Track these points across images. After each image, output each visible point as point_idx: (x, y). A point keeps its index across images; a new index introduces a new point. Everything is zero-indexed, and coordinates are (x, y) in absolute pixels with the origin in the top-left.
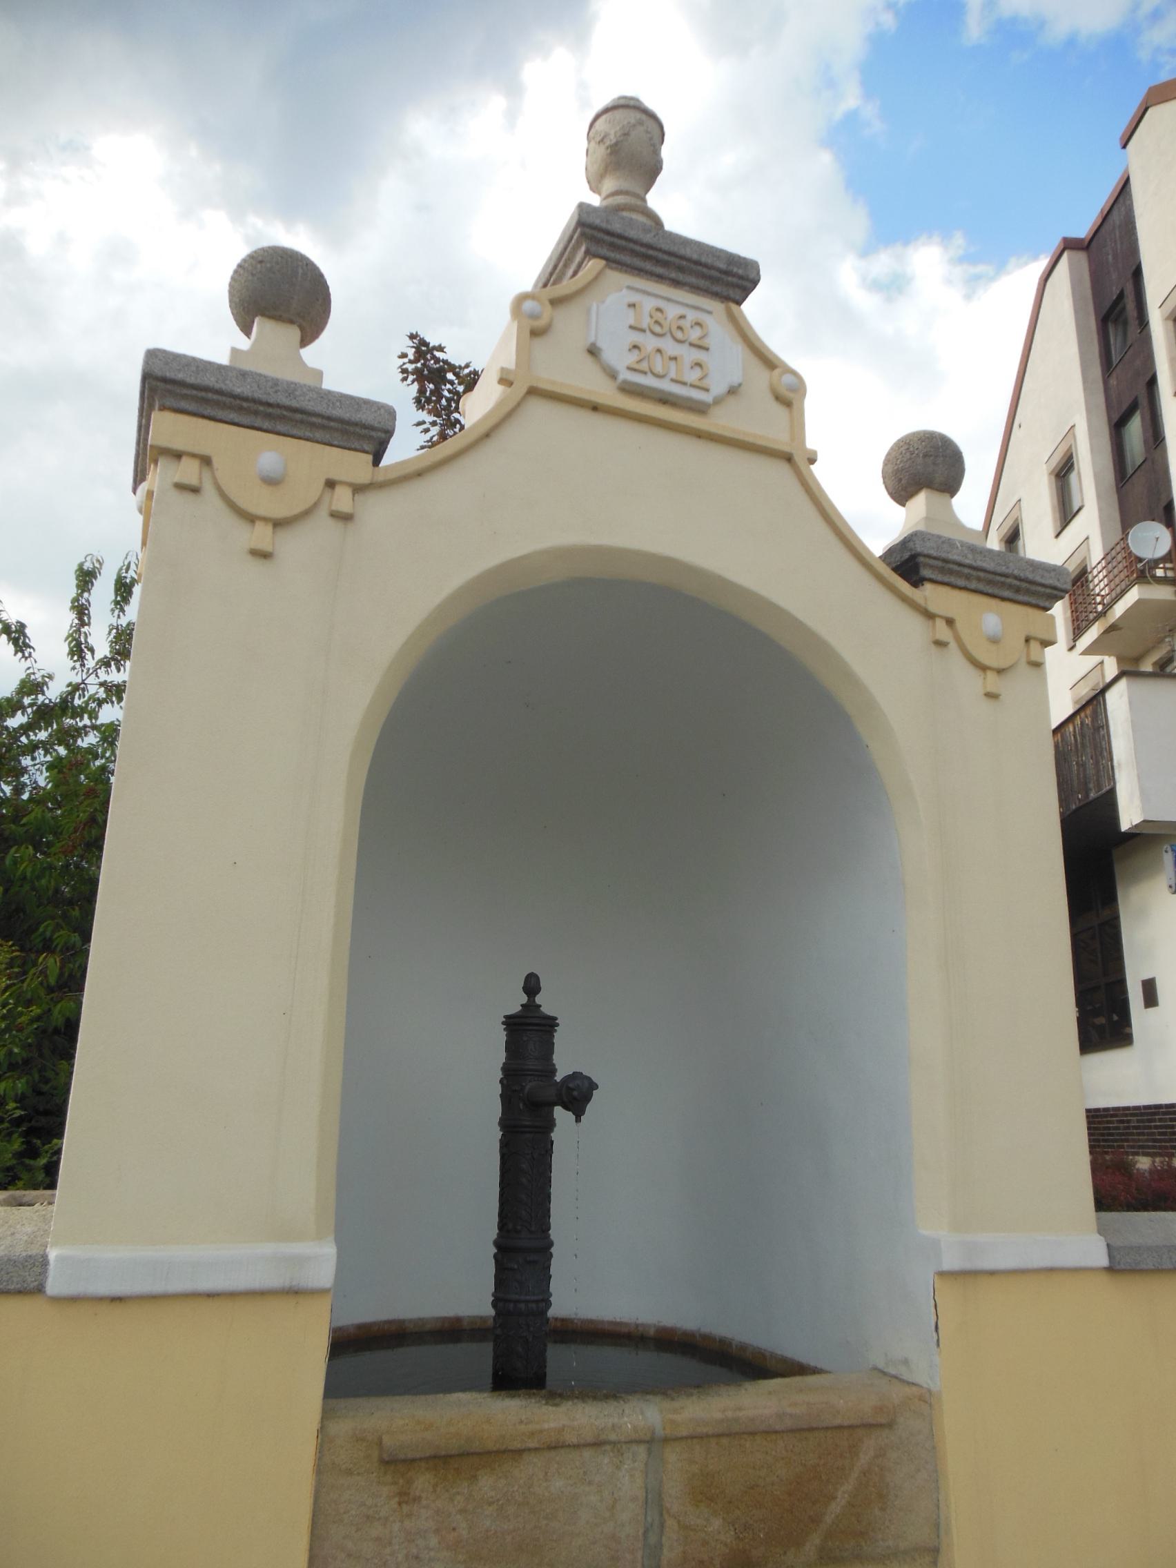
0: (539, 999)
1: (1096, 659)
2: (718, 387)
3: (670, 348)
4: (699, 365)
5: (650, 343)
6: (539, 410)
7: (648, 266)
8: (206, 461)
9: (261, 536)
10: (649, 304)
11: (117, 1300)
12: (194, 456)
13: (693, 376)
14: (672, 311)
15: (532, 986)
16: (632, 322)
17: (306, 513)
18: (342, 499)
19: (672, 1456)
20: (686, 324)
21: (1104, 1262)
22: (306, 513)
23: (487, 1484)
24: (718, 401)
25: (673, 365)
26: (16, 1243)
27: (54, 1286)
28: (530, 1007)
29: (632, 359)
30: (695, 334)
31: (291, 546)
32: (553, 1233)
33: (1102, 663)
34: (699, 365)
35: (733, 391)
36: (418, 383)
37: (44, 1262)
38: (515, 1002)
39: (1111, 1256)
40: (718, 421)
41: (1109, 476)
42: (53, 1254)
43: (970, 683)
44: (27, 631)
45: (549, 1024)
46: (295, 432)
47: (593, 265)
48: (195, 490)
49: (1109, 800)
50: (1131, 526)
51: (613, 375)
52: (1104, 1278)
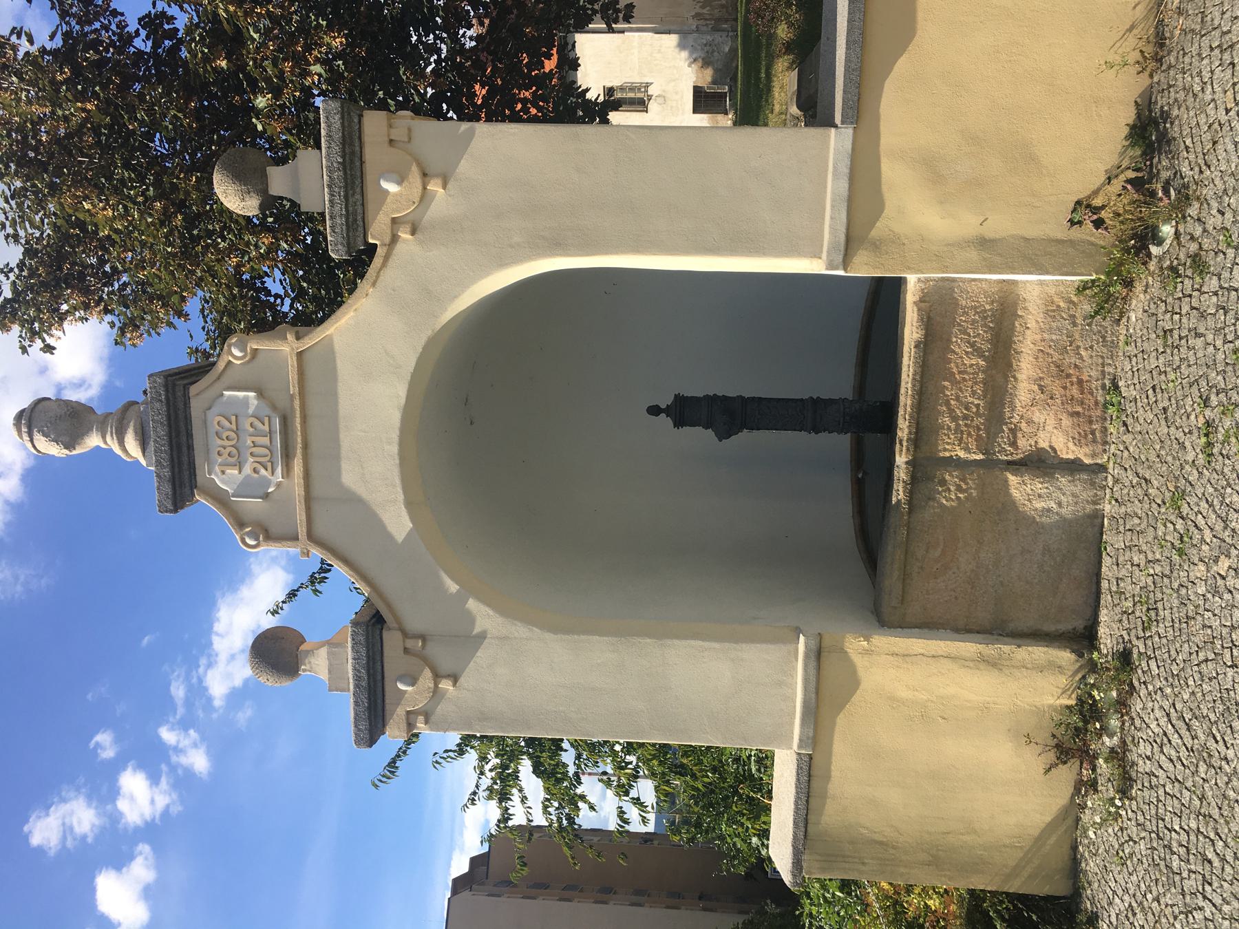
0: (663, 406)
15: (654, 410)
26: (637, 802)
28: (668, 411)
32: (806, 397)
36: (390, 537)
38: (665, 421)
45: (678, 398)
46: (380, 670)
50: (834, 123)
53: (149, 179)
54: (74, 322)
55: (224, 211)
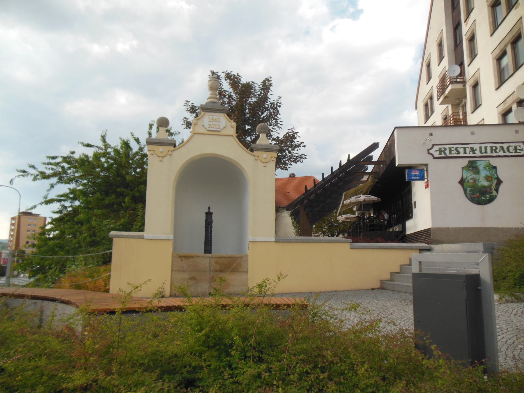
1: (445, 106)
2: (222, 127)
3: (214, 123)
4: (219, 125)
5: (211, 123)
6: (196, 136)
7: (212, 111)
8: (154, 150)
9: (161, 159)
10: (211, 117)
11: (151, 239)
12: (152, 150)
13: (218, 127)
14: (215, 117)
15: (209, 208)
16: (209, 120)
17: (166, 155)
18: (170, 153)
19: (213, 259)
20: (217, 119)
21: (273, 239)
22: (166, 155)
23: (191, 260)
24: (222, 129)
25: (215, 126)
27: (145, 238)
28: (209, 211)
29: (209, 126)
30: (218, 120)
31: (165, 159)
33: (448, 106)
34: (219, 125)
35: (224, 127)
37: (144, 236)
38: (207, 211)
39: (400, 269)
40: (223, 132)
41: (452, 46)
42: (145, 235)
43: (261, 165)
44: (139, 139)
45: (212, 214)
47: (203, 113)
48: (153, 154)
49: (394, 160)
51: (206, 129)
52: (275, 243)
53: (325, 229)
54: (275, 102)
55: (256, 126)
